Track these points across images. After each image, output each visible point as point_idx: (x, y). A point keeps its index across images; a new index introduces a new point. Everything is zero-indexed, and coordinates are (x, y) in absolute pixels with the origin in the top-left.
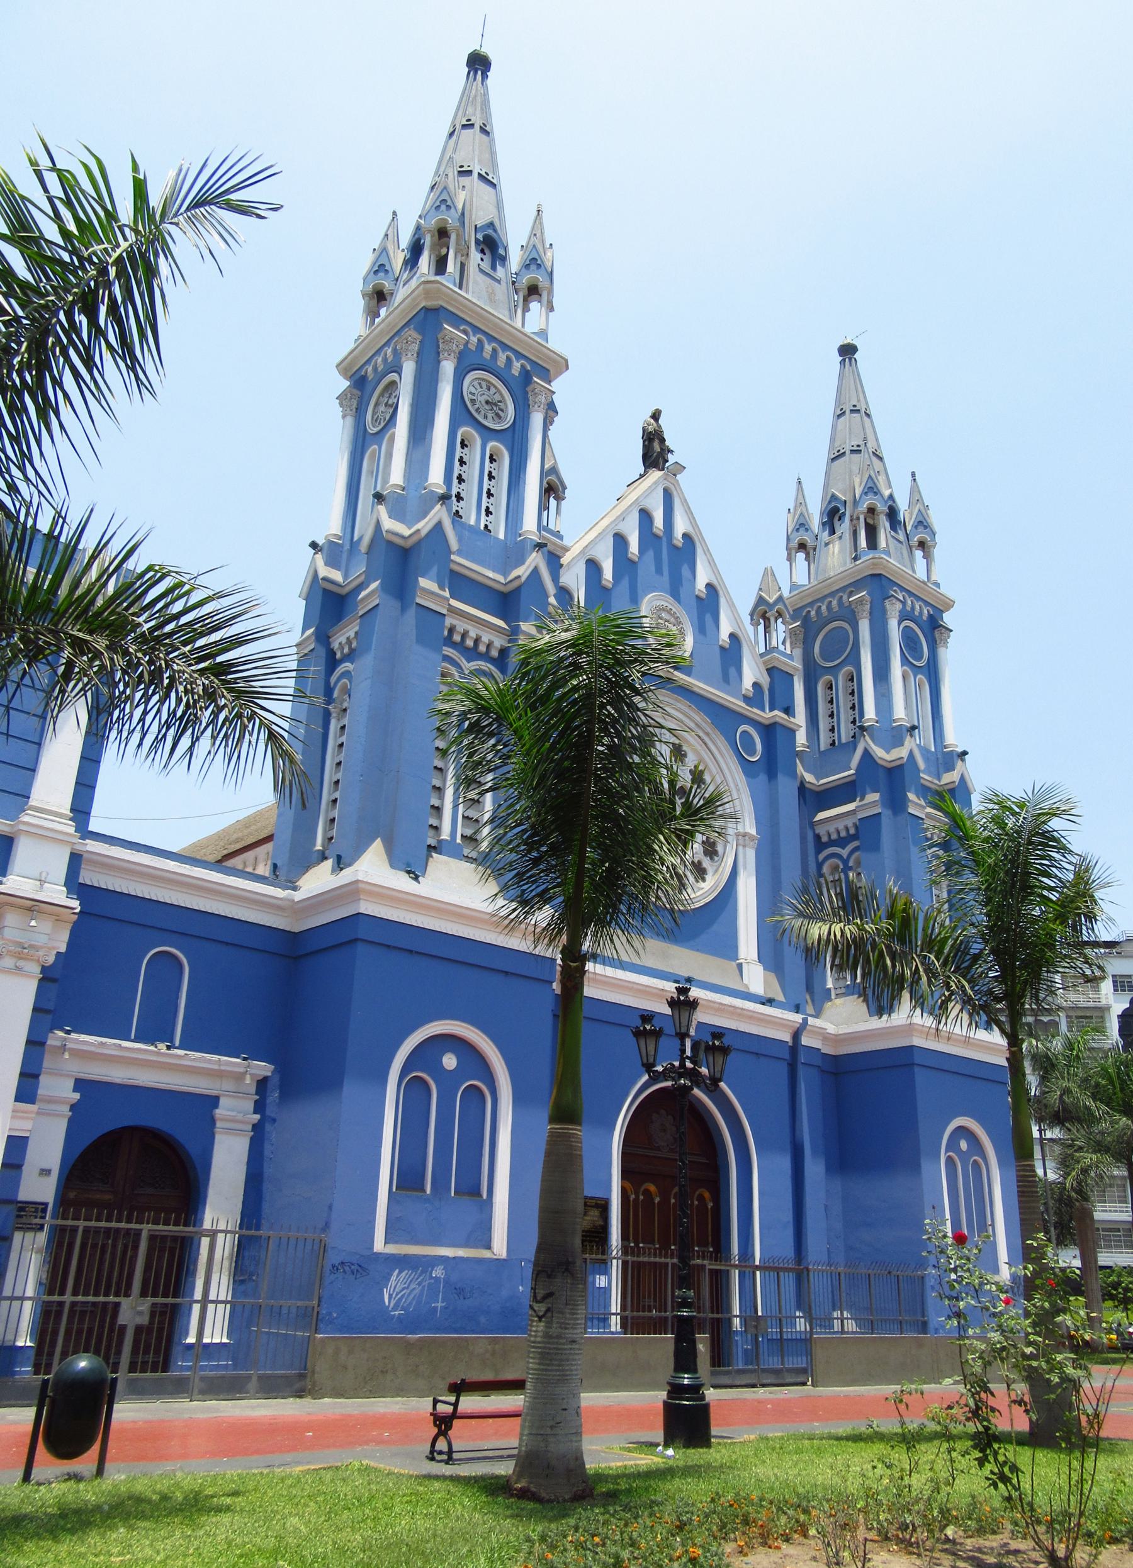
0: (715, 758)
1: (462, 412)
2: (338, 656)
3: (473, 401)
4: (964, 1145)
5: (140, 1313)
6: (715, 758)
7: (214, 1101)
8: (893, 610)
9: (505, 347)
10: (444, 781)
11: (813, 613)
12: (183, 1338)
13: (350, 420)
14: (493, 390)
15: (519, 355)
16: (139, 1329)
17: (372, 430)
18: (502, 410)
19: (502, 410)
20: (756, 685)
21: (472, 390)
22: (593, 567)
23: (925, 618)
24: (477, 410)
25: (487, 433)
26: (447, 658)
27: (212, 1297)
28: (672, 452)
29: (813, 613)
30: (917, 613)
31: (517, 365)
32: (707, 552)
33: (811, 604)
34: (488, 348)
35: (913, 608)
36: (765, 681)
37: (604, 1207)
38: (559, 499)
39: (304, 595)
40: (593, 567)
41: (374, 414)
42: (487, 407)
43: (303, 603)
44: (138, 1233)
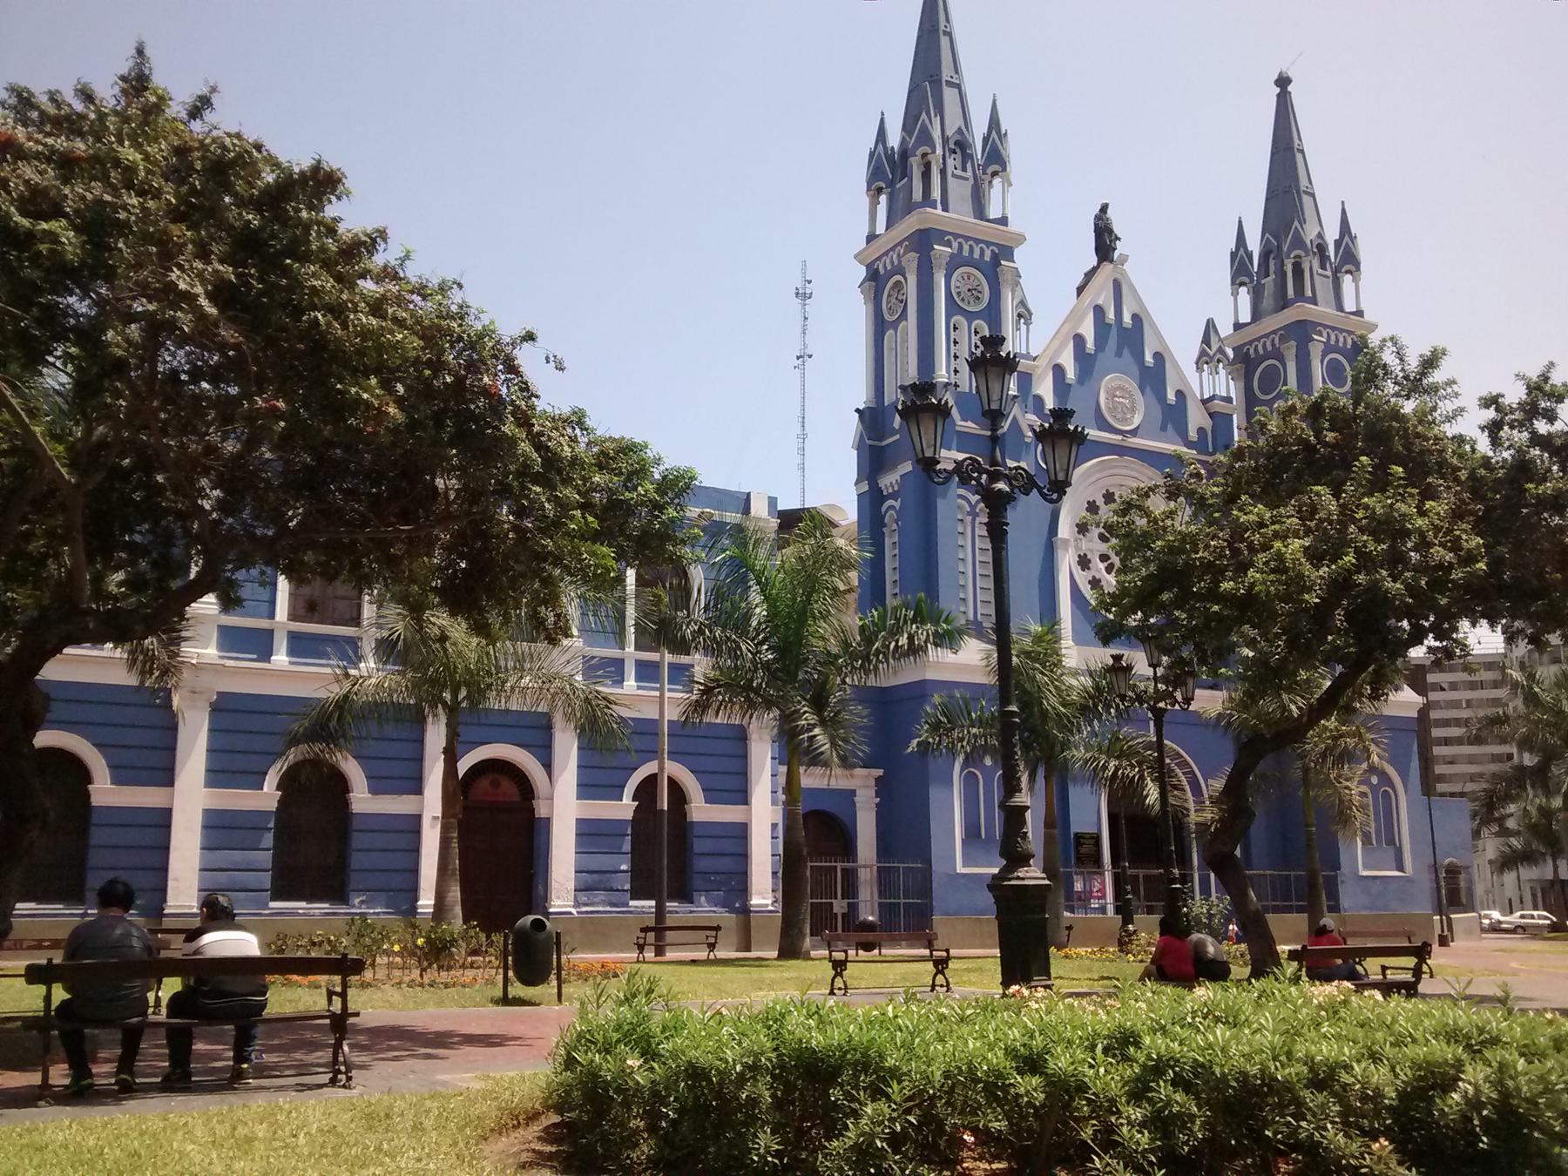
0: (979, 957)
1: (953, 307)
2: (885, 493)
3: (959, 293)
4: (1374, 780)
5: (842, 907)
6: (979, 957)
7: (853, 793)
8: (1316, 350)
9: (978, 241)
10: (966, 580)
11: (1252, 351)
12: (1509, 774)
13: (871, 306)
14: (972, 278)
15: (989, 244)
16: (843, 914)
17: (887, 317)
18: (980, 292)
19: (980, 292)
20: (1201, 430)
21: (958, 284)
22: (1058, 370)
23: (1349, 347)
24: (963, 300)
25: (971, 315)
26: (961, 496)
27: (868, 903)
28: (1119, 239)
29: (1252, 351)
30: (1341, 345)
31: (988, 254)
32: (1153, 325)
33: (1250, 343)
34: (966, 247)
35: (1337, 341)
36: (1207, 423)
37: (1097, 839)
38: (1028, 324)
39: (856, 446)
40: (1058, 370)
41: (888, 303)
42: (969, 294)
43: (855, 452)
44: (836, 867)
